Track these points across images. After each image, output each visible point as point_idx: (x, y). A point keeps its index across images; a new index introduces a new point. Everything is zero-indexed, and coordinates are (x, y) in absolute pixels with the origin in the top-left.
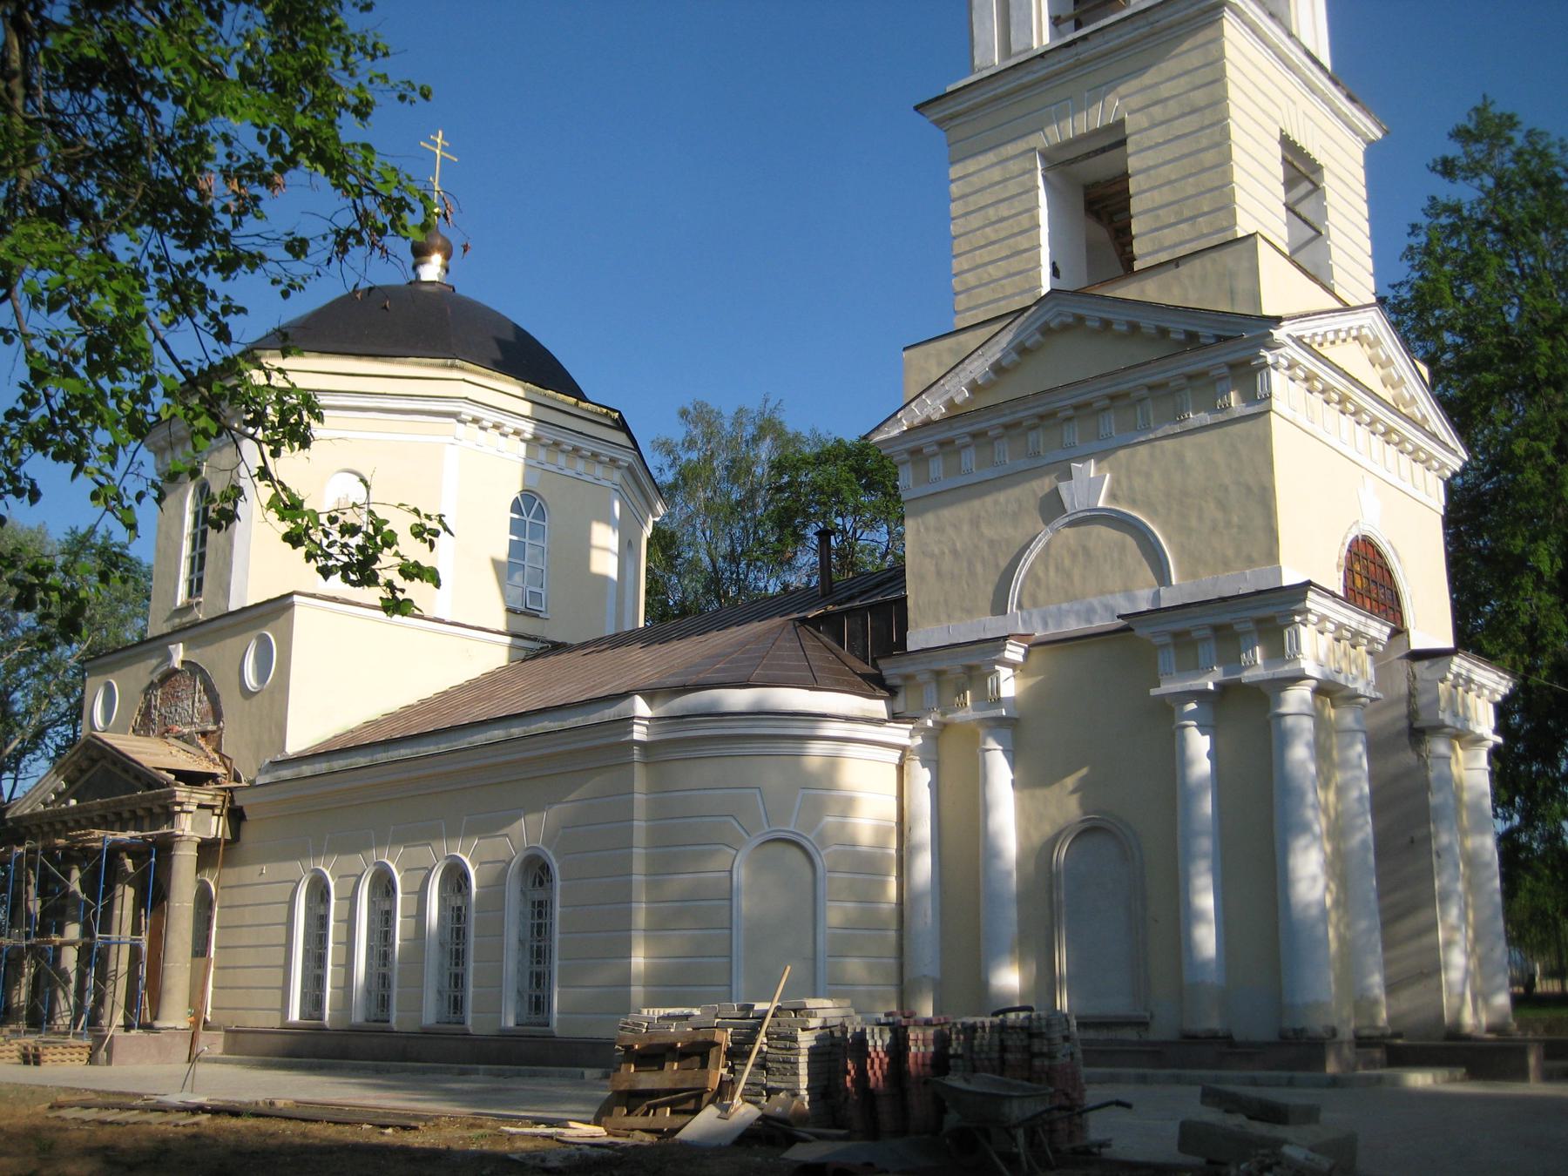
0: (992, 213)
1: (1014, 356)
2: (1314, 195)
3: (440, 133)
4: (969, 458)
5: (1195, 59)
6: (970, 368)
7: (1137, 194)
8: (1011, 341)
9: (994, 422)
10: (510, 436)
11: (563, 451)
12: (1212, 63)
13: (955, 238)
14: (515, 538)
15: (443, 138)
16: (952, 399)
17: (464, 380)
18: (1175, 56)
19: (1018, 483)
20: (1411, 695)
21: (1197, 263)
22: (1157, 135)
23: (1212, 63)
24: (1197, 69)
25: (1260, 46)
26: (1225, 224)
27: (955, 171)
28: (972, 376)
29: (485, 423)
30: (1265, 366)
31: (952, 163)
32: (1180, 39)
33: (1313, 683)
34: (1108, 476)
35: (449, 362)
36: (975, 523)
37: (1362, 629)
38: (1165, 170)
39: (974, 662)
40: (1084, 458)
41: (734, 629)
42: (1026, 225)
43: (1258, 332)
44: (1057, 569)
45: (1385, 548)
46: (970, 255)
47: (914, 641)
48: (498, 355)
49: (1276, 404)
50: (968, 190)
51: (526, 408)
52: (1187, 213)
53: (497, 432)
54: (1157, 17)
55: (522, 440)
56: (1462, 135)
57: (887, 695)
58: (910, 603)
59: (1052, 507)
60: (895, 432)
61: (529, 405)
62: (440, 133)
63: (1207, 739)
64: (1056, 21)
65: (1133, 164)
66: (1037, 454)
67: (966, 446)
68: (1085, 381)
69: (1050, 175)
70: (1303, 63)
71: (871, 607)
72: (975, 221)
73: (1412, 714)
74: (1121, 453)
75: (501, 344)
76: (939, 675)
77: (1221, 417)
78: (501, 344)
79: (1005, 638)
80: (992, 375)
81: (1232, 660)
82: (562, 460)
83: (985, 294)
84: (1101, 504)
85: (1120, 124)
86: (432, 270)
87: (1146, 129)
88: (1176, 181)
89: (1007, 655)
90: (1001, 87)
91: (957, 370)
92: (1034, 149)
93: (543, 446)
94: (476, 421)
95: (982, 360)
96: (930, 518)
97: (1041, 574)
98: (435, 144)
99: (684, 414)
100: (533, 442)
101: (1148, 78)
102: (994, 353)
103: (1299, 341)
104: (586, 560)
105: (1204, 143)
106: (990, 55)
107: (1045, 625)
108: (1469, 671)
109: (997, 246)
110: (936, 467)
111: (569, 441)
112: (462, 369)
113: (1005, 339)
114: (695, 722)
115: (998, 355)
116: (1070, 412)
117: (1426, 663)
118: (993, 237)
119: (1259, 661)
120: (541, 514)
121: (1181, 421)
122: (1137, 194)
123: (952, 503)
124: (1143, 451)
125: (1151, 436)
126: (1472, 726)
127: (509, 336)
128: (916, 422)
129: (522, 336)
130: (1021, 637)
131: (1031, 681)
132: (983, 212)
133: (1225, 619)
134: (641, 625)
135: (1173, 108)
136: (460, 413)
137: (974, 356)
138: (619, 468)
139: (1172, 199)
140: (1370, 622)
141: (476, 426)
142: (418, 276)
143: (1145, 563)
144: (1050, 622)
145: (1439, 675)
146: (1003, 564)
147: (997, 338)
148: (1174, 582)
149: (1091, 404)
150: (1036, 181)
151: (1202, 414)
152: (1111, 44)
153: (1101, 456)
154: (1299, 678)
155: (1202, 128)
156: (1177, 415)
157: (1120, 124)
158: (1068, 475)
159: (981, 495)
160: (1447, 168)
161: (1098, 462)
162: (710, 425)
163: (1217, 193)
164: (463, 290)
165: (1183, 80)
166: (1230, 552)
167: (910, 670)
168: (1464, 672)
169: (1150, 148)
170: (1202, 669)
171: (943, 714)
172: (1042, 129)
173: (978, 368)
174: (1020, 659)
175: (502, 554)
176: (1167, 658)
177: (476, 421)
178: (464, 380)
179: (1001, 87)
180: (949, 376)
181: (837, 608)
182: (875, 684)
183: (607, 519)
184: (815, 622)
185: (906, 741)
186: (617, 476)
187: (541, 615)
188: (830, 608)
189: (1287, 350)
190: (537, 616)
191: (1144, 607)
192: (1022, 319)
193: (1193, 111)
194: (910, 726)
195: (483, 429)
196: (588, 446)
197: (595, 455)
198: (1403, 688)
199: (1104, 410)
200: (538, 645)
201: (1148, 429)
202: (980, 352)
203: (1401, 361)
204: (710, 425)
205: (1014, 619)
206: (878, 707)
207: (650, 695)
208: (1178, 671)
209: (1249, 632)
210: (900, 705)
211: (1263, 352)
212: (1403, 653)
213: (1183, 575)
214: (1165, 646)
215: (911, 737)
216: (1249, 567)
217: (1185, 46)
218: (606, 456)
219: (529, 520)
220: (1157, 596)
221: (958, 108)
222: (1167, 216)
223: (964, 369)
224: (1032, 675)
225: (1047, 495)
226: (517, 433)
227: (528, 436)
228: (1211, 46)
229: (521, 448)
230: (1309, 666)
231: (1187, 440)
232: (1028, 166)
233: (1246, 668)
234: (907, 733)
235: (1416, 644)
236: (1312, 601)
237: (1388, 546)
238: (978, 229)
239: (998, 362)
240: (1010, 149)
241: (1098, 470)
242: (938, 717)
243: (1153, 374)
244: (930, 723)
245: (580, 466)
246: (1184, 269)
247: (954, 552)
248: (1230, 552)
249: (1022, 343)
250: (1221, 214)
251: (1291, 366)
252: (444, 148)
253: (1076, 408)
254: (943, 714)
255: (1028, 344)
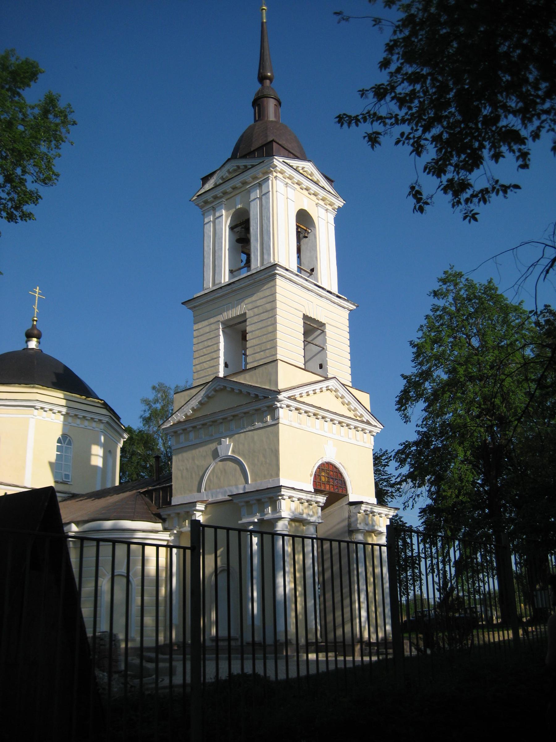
0: (206, 344)
1: (206, 399)
2: (322, 334)
3: (38, 287)
4: (192, 435)
5: (267, 293)
6: (192, 403)
7: (250, 340)
8: (204, 395)
9: (198, 423)
10: (57, 413)
11: (79, 418)
12: (273, 294)
13: (194, 352)
14: (59, 453)
15: (39, 290)
16: (186, 414)
17: (37, 393)
18: (262, 291)
19: (206, 445)
20: (349, 517)
21: (261, 369)
22: (255, 319)
23: (273, 294)
24: (268, 296)
25: (295, 285)
26: (274, 353)
27: (196, 327)
28: (192, 406)
29: (46, 409)
30: (277, 408)
31: (195, 324)
32: (264, 284)
33: (288, 519)
34: (232, 444)
35: (32, 385)
36: (193, 459)
37: (310, 499)
38: (257, 332)
39: (188, 510)
40: (225, 437)
41: (121, 494)
42: (216, 349)
43: (275, 396)
44: (216, 477)
45: (338, 465)
46: (198, 359)
47: (175, 501)
48: (55, 380)
49: (281, 421)
50: (199, 334)
51: (63, 402)
52: (263, 349)
53: (51, 412)
54: (255, 277)
55: (62, 415)
56: (444, 281)
57: (162, 521)
58: (173, 487)
59: (215, 454)
60: (168, 425)
61: (65, 401)
62: (38, 287)
63: (256, 538)
64: (231, 272)
65: (248, 329)
66: (212, 435)
67: (191, 431)
68: (224, 410)
69: (226, 330)
70: (314, 288)
71: (162, 488)
72: (201, 346)
73: (349, 525)
74: (236, 436)
75: (57, 375)
76: (178, 514)
77: (265, 425)
78: (57, 375)
79: (196, 502)
80: (199, 406)
81: (262, 512)
82: (78, 421)
83: (202, 374)
84: (229, 454)
85: (245, 314)
86: (33, 344)
87: (252, 317)
88: (260, 336)
89: (197, 508)
90: (209, 298)
91: (187, 404)
92: (219, 321)
93: (71, 416)
94: (42, 408)
95: (195, 400)
96: (180, 456)
97: (212, 478)
98: (35, 292)
99: (154, 388)
100: (66, 415)
101: (254, 298)
102: (199, 398)
103: (289, 398)
104: (89, 460)
105: (269, 323)
106: (209, 285)
107: (212, 497)
108: (371, 508)
109: (207, 356)
110: (182, 438)
111: (81, 414)
112: (37, 388)
113: (202, 393)
114: (88, 533)
115: (201, 399)
116: (221, 421)
117: (354, 506)
118: (206, 353)
119: (270, 512)
120: (70, 443)
121: (254, 425)
122: (250, 340)
123: (186, 451)
124: (242, 435)
125: (245, 430)
126: (376, 528)
127: (61, 371)
128: (175, 422)
129: (67, 370)
130: (202, 502)
131: (207, 517)
132: (203, 343)
133: (259, 497)
134: (117, 484)
135: (261, 310)
136: (35, 406)
137: (192, 399)
138: (103, 423)
139: (258, 343)
140: (316, 496)
141: (42, 410)
142: (27, 346)
143: (242, 476)
144: (214, 496)
145: (358, 511)
146: (201, 474)
147: (199, 393)
148: (250, 483)
149: (216, 421)
150: (219, 333)
151: (260, 423)
152: (242, 285)
153: (230, 436)
154: (281, 518)
155: (269, 318)
156: (252, 424)
157: (245, 314)
158: (220, 443)
159: (195, 449)
160: (436, 294)
161: (230, 438)
162: (164, 392)
163: (272, 342)
164: (46, 351)
165: (264, 299)
166: (266, 473)
167: (169, 512)
168: (369, 509)
169: (254, 323)
170: (254, 515)
171: (180, 528)
172: (222, 314)
173: (194, 403)
174: (203, 509)
175: (53, 459)
176: (244, 510)
177: (42, 408)
178: (37, 393)
179: (209, 298)
180: (185, 406)
181: (153, 488)
182: (158, 517)
183: (98, 443)
184: (144, 493)
185: (169, 538)
186: (102, 426)
187: (69, 483)
188: (150, 488)
189: (285, 401)
190: (67, 484)
191: (241, 492)
192: (207, 386)
193: (266, 311)
194: (169, 533)
195: (46, 411)
196: (89, 416)
197: (92, 419)
198: (347, 515)
199: (231, 420)
200: (67, 495)
201: (244, 428)
202: (194, 398)
203: (349, 396)
204: (164, 392)
205: (204, 495)
206: (159, 526)
207: (77, 523)
208: (248, 515)
209: (266, 502)
210: (167, 525)
211: (276, 403)
212: (347, 503)
213: (252, 480)
214: (243, 506)
215: (170, 536)
216: (271, 478)
217: (265, 287)
218: (97, 419)
219: (65, 445)
220: (245, 487)
221: (195, 304)
222: (257, 349)
223: (190, 404)
224: (207, 515)
225: (214, 450)
226: (59, 412)
227: (64, 413)
228: (272, 288)
229: (62, 418)
230: (284, 514)
231: (255, 432)
232: (217, 327)
233: (266, 514)
234: (168, 535)
235: (351, 500)
236: (284, 491)
237: (340, 465)
238: (201, 349)
239: (200, 401)
240: (212, 320)
241: (229, 442)
242: (178, 530)
243: (244, 409)
244: (175, 532)
245: (86, 423)
246: (257, 371)
247: (187, 469)
248: (266, 473)
249: (208, 395)
250: (272, 349)
251: (288, 406)
252: (39, 294)
253: (223, 419)
254: (180, 528)
255: (210, 395)
